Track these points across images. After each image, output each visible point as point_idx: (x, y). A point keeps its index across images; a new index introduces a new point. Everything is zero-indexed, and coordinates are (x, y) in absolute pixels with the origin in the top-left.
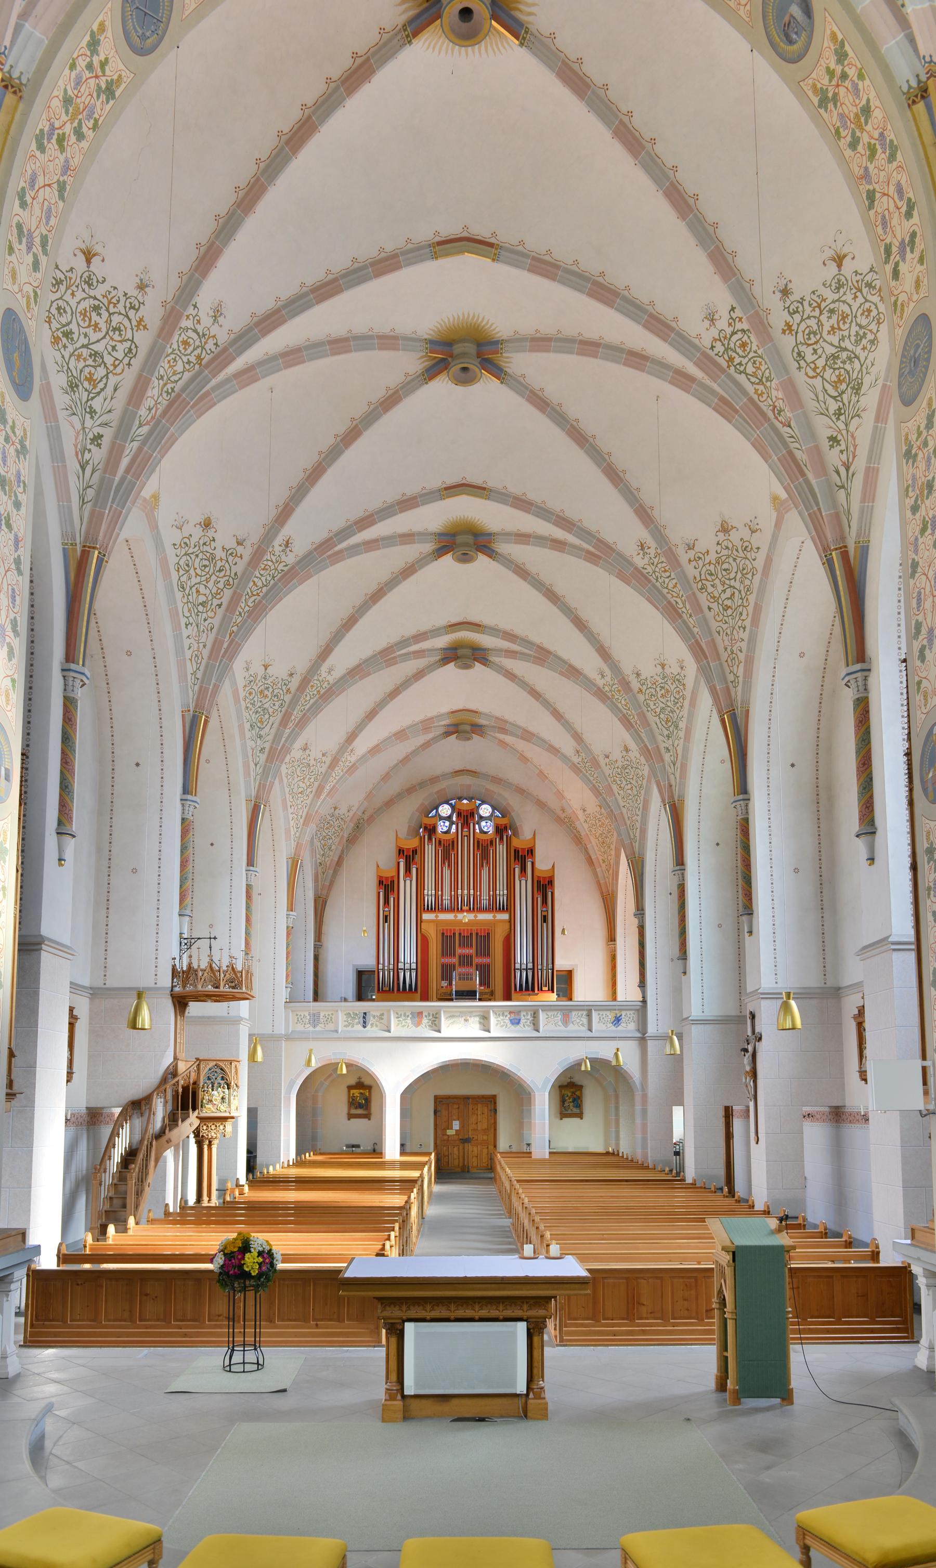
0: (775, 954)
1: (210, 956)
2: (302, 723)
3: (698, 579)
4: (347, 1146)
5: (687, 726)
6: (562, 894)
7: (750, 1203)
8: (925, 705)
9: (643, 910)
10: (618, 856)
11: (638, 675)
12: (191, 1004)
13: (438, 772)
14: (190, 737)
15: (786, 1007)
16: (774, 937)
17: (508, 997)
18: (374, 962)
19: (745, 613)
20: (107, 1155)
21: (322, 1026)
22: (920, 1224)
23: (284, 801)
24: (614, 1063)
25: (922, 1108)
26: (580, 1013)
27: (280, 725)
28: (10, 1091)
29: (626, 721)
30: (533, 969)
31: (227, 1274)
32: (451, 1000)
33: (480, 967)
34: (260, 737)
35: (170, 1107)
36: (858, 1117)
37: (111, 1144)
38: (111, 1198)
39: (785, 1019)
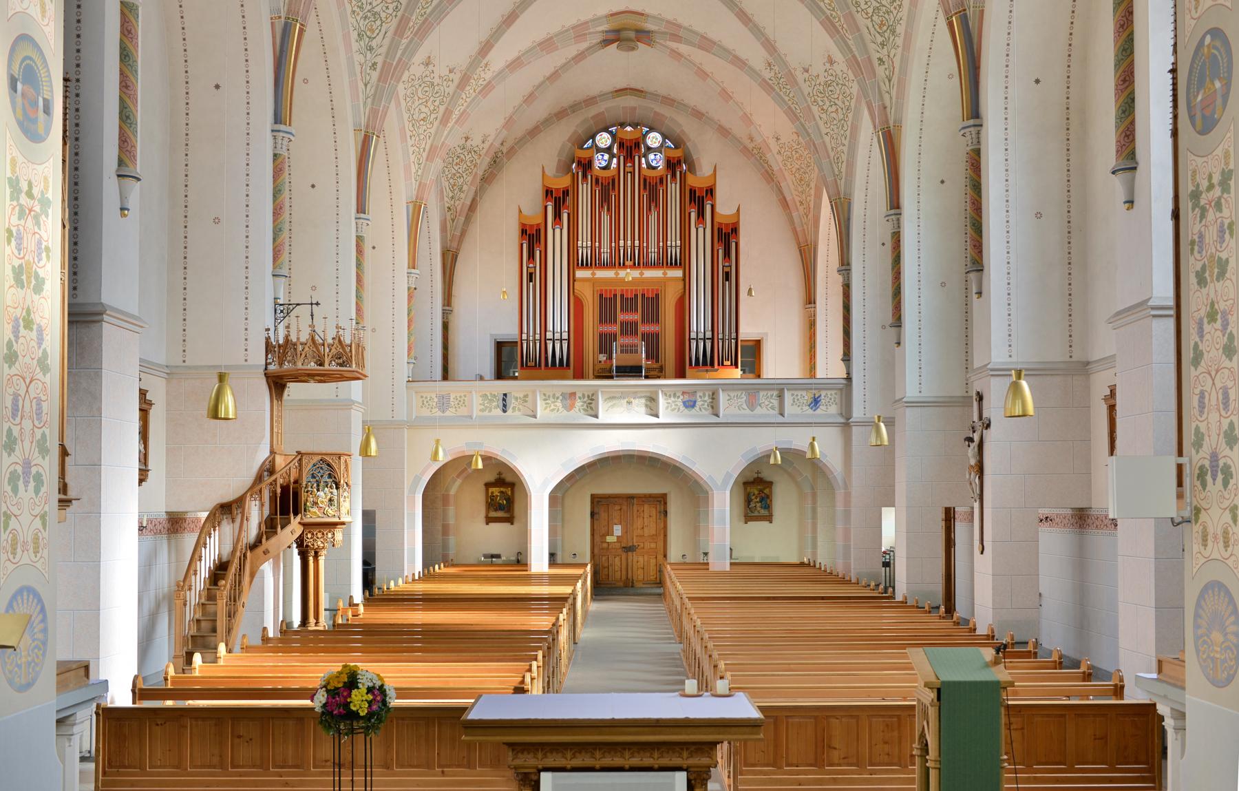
0: (1010, 320)
1: (312, 326)
2: (424, 30)
4: (485, 556)
5: (906, 31)
6: (747, 241)
7: (971, 625)
8: (1196, 8)
9: (848, 264)
10: (818, 197)
12: (289, 385)
13: (595, 90)
14: (282, 51)
15: (1016, 388)
16: (1009, 299)
17: (681, 374)
18: (516, 331)
20: (191, 569)
21: (453, 410)
22: (1167, 656)
23: (403, 130)
24: (809, 455)
25: (1174, 515)
26: (770, 393)
27: (395, 34)
28: (63, 497)
29: (830, 25)
30: (712, 339)
31: (330, 713)
32: (611, 377)
33: (645, 337)
34: (371, 49)
35: (266, 512)
36: (1106, 522)
37: (196, 556)
38: (198, 621)
39: (1014, 404)
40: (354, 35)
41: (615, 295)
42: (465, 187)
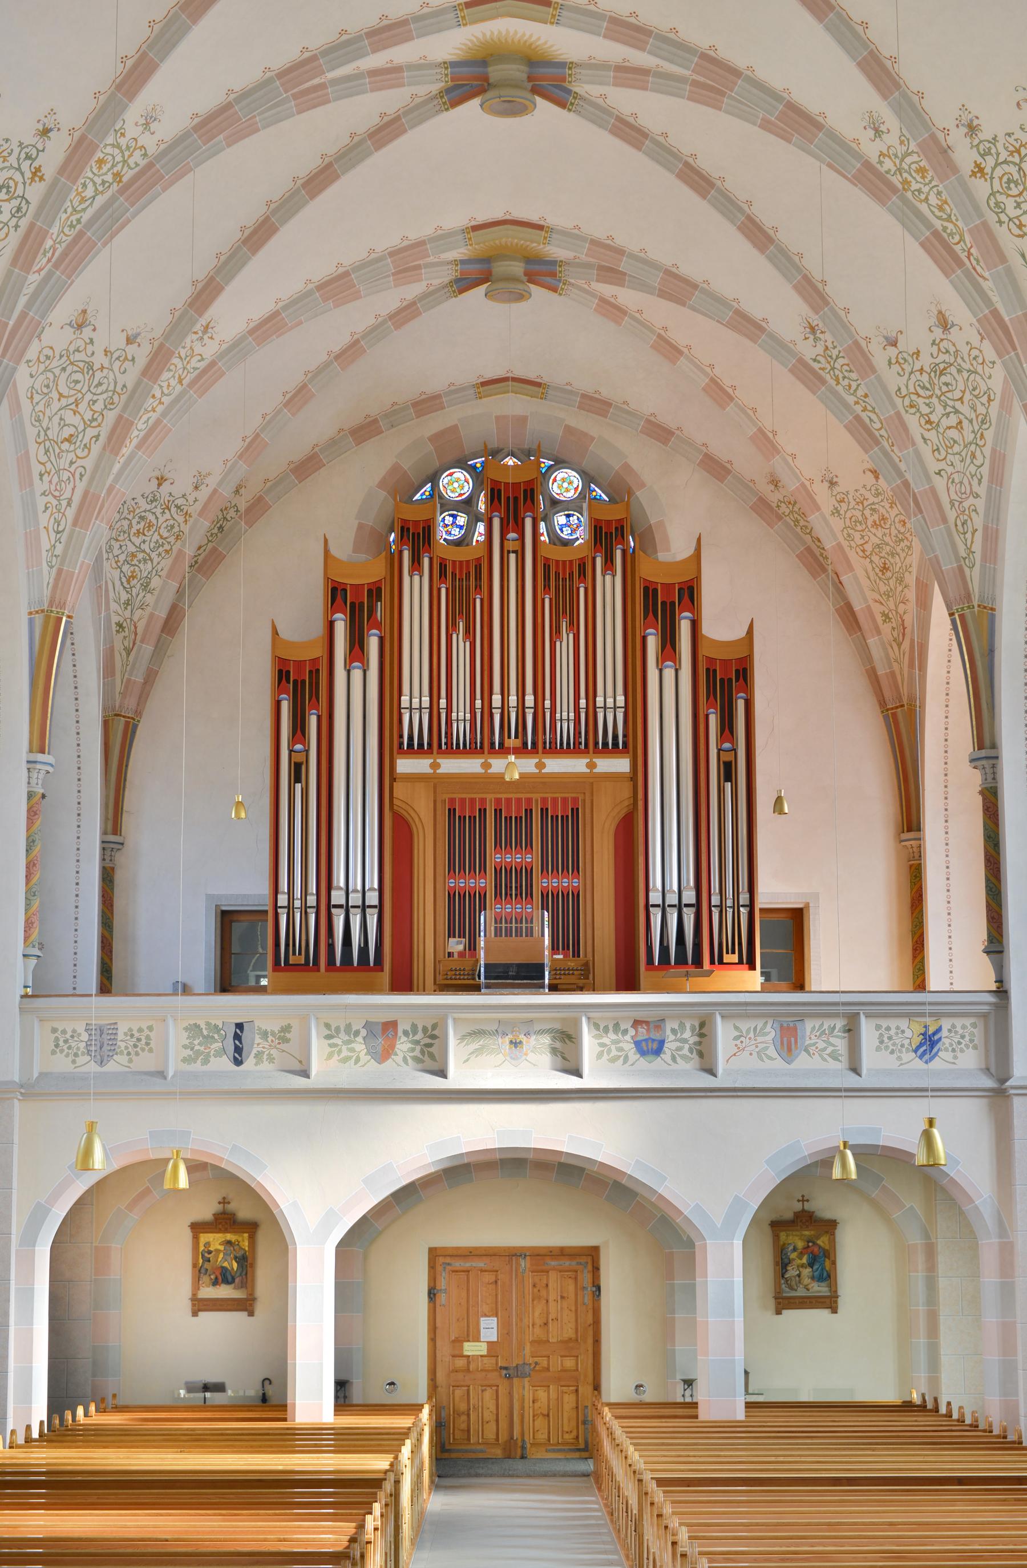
3: (904, 392)
9: (994, 746)
11: (972, 129)
19: (978, 453)
26: (828, 1023)
42: (156, 582)
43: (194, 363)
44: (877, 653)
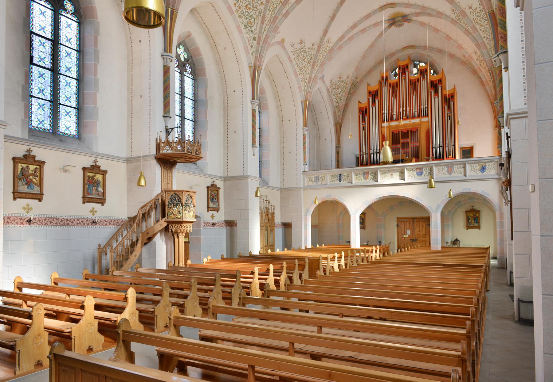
6: (460, 103)
13: (394, 50)
26: (459, 166)
34: (252, 32)
40: (242, 27)
41: (399, 132)
42: (342, 98)
43: (328, 48)
44: (488, 89)
